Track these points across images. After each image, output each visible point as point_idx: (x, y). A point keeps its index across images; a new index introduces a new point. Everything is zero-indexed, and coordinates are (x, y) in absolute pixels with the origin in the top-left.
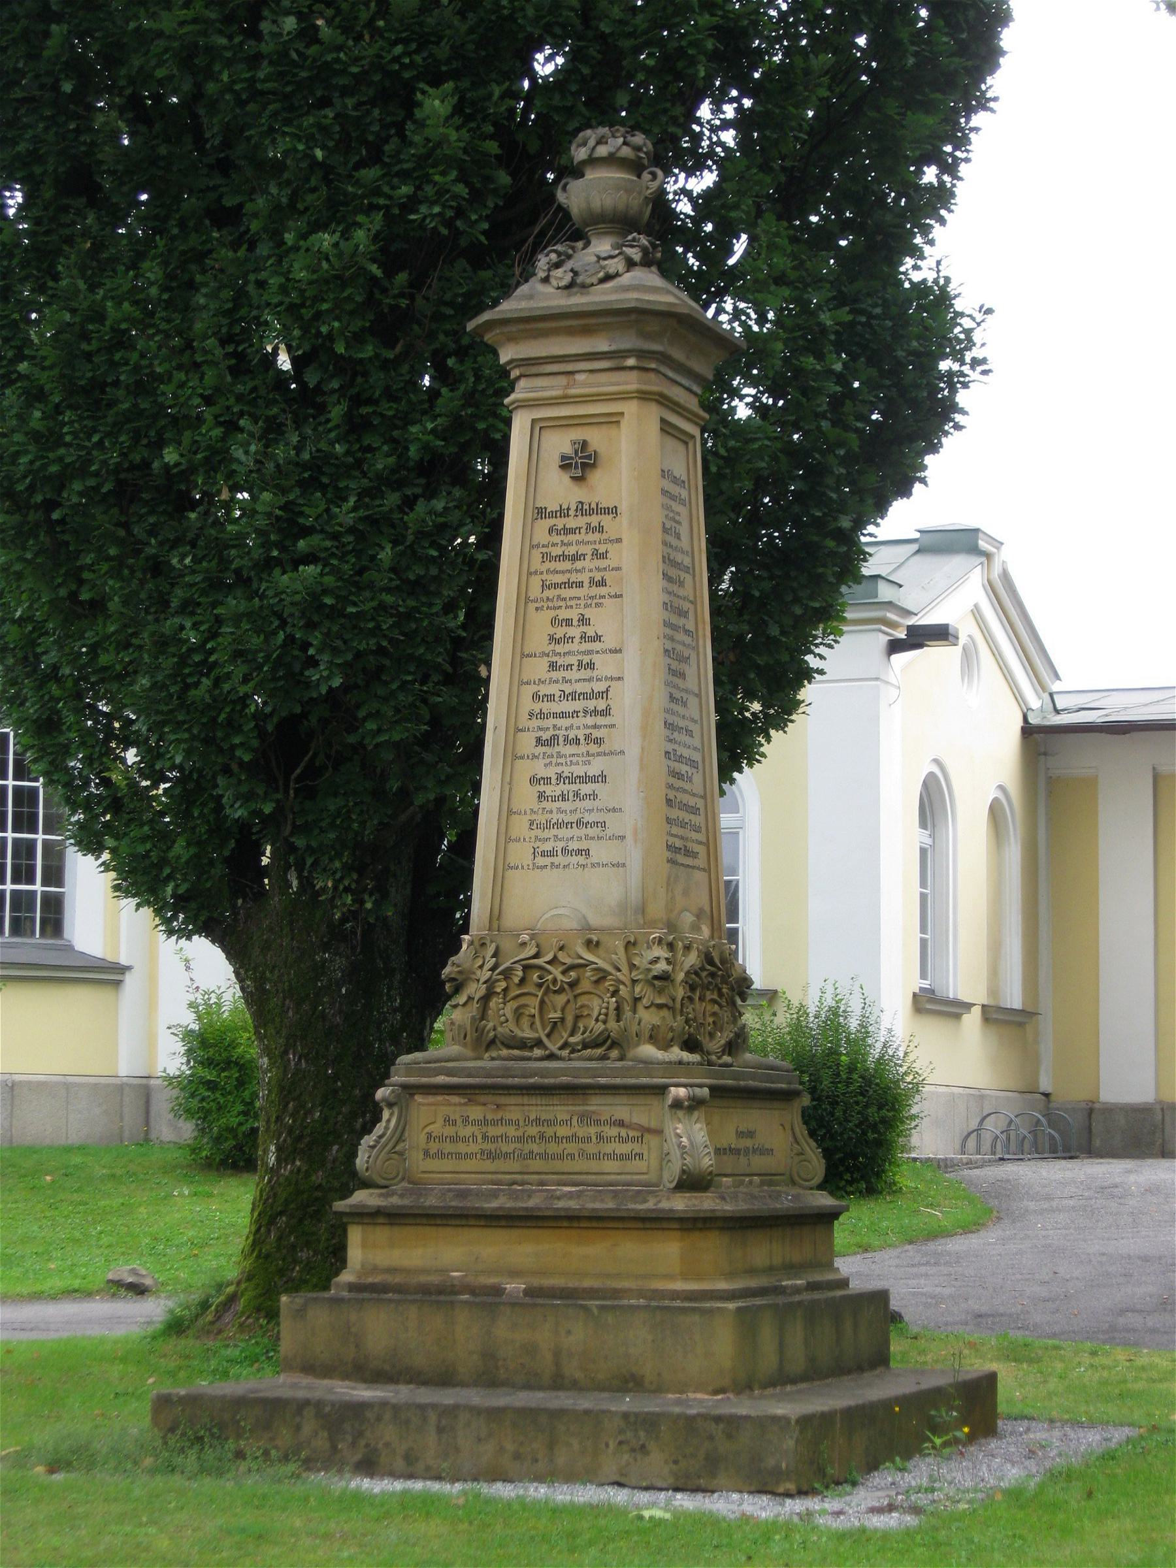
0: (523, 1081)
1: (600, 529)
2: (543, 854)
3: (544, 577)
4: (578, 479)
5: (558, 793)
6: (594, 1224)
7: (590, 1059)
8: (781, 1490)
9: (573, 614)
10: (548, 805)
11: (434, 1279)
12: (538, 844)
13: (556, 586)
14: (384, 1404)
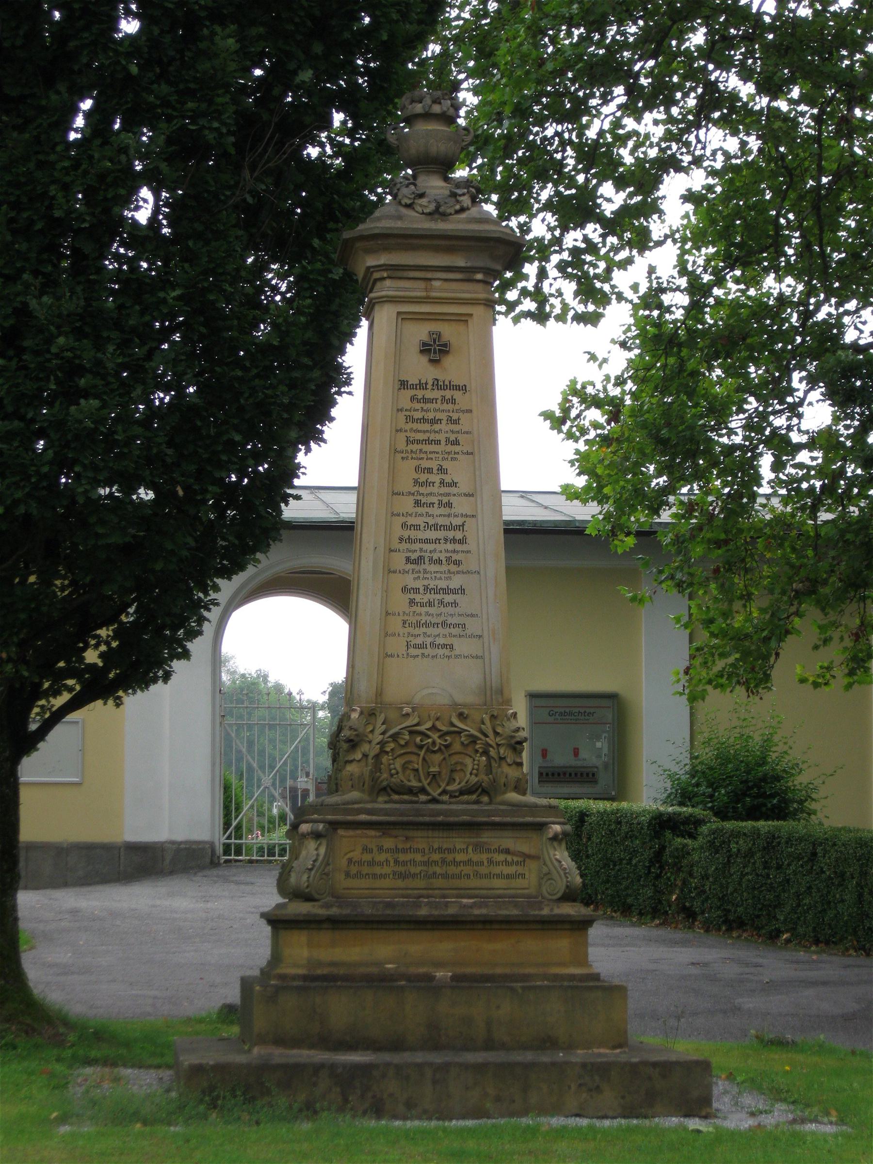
0: (432, 819)
1: (453, 401)
2: (416, 646)
3: (408, 434)
4: (434, 362)
5: (426, 600)
6: (503, 926)
7: (468, 803)
8: (704, 1113)
9: (434, 465)
10: (418, 609)
11: (374, 970)
12: (410, 638)
13: (418, 442)
14: (388, 1065)
